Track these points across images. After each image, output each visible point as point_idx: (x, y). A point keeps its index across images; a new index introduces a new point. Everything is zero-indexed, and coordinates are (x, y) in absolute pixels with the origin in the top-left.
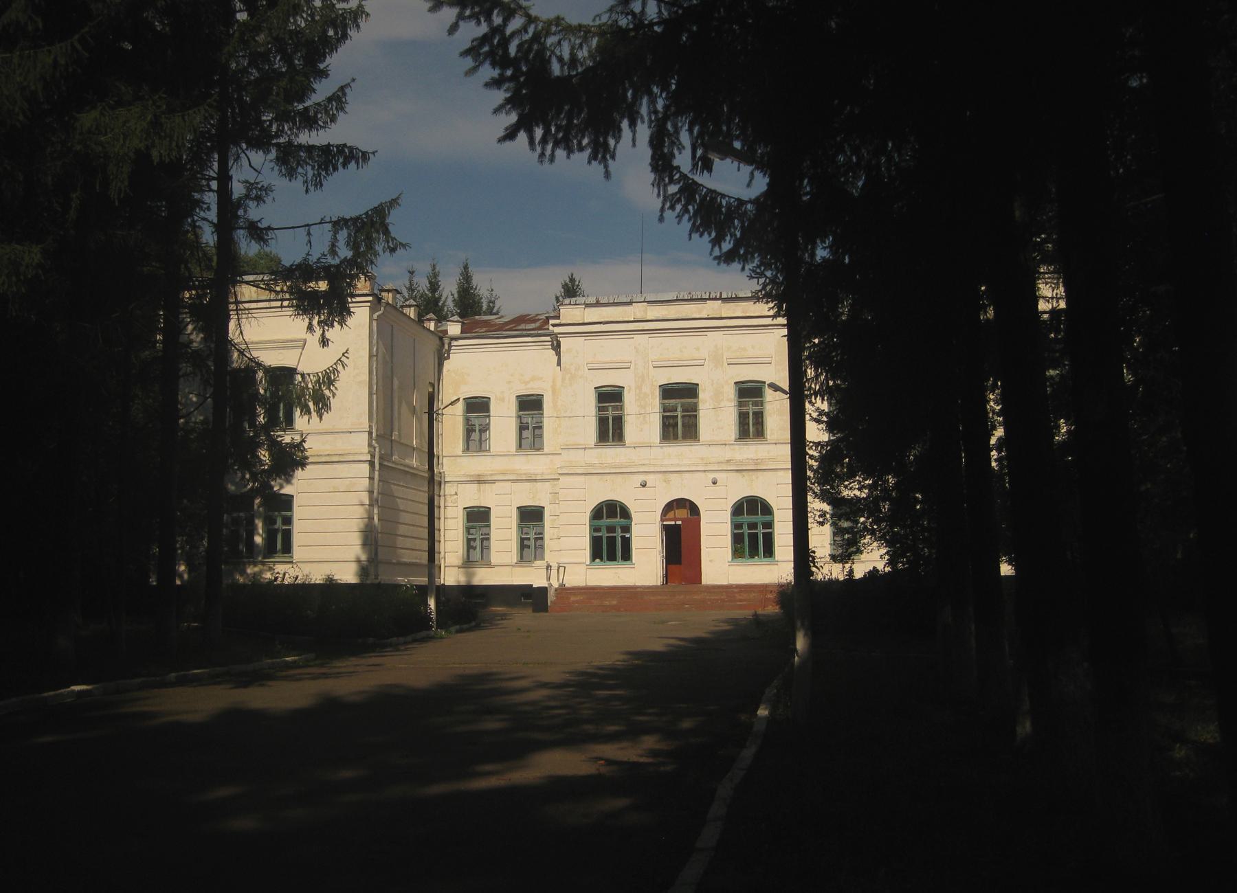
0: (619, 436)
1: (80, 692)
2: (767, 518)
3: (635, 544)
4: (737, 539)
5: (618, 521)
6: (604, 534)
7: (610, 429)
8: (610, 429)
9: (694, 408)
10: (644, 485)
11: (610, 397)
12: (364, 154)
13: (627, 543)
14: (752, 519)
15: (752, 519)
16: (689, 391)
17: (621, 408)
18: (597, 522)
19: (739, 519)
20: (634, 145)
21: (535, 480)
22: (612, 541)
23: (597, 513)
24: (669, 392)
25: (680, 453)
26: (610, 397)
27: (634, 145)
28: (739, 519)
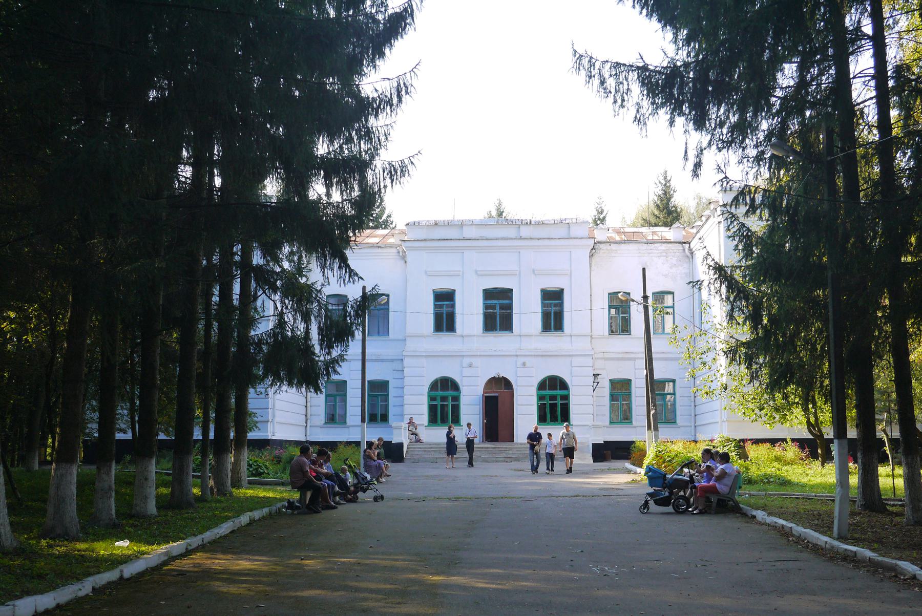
0: (451, 327)
1: (438, 574)
2: (564, 392)
3: (573, 409)
4: (432, 409)
5: (450, 393)
6: (438, 403)
7: (445, 321)
8: (445, 321)
9: (510, 307)
10: (524, 364)
11: (444, 298)
12: (405, 10)
13: (456, 409)
14: (445, 393)
15: (445, 393)
16: (506, 294)
17: (453, 306)
18: (434, 393)
19: (434, 393)
20: (644, 269)
21: (382, 361)
22: (553, 406)
23: (434, 386)
24: (489, 294)
25: (499, 341)
26: (444, 298)
27: (644, 269)
28: (543, 393)
